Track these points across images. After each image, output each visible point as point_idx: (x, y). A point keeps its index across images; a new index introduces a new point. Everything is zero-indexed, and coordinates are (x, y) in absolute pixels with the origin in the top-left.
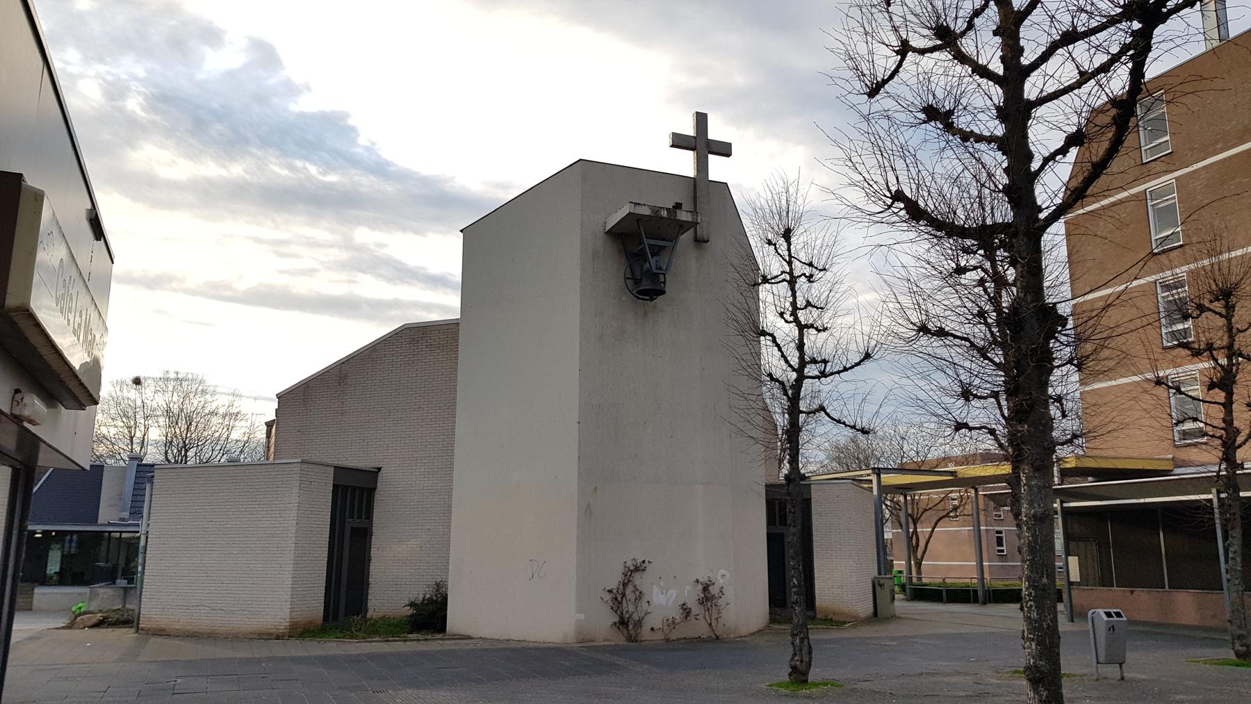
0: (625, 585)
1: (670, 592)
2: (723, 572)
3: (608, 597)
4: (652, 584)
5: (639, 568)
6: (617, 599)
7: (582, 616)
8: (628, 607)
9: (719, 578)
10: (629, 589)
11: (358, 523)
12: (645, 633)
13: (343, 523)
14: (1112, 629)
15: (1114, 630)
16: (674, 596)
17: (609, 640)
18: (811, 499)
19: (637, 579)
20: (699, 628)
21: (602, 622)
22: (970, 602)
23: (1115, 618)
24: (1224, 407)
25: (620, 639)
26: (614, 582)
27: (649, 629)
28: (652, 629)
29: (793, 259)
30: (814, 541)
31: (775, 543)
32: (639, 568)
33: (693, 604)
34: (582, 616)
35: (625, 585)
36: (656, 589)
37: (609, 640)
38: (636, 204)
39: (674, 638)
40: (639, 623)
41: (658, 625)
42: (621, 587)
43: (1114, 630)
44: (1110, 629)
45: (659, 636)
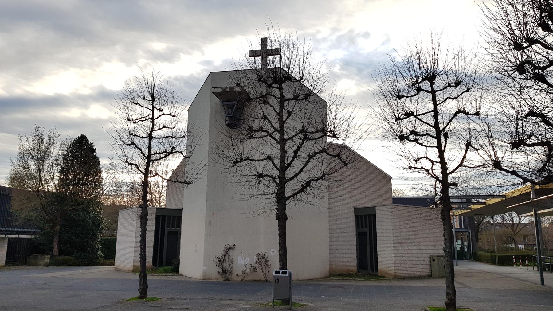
0: (225, 255)
1: (246, 259)
2: (273, 250)
3: (217, 260)
4: (238, 255)
5: (232, 248)
6: (221, 261)
7: (206, 269)
8: (227, 265)
9: (271, 253)
10: (227, 257)
11: (173, 230)
12: (234, 277)
13: (163, 229)
14: (277, 280)
15: (278, 281)
16: (248, 261)
17: (217, 279)
18: (375, 214)
19: (230, 253)
20: (259, 275)
21: (214, 272)
22: (496, 265)
23: (281, 275)
24: (440, 163)
25: (221, 279)
26: (220, 253)
27: (236, 276)
28: (237, 275)
29: (152, 109)
30: (377, 236)
31: (360, 236)
32: (232, 248)
33: (256, 265)
34: (206, 269)
35: (225, 255)
36: (239, 257)
37: (217, 279)
38: (215, 88)
39: (248, 279)
40: (231, 273)
41: (240, 273)
42: (223, 257)
43: (278, 281)
44: (275, 280)
45: (240, 279)
